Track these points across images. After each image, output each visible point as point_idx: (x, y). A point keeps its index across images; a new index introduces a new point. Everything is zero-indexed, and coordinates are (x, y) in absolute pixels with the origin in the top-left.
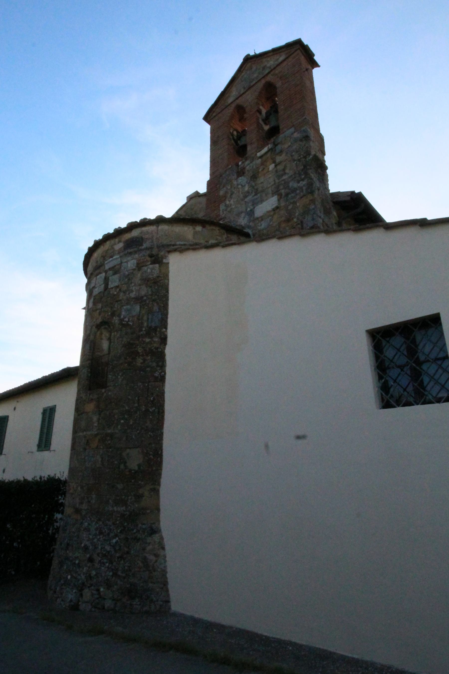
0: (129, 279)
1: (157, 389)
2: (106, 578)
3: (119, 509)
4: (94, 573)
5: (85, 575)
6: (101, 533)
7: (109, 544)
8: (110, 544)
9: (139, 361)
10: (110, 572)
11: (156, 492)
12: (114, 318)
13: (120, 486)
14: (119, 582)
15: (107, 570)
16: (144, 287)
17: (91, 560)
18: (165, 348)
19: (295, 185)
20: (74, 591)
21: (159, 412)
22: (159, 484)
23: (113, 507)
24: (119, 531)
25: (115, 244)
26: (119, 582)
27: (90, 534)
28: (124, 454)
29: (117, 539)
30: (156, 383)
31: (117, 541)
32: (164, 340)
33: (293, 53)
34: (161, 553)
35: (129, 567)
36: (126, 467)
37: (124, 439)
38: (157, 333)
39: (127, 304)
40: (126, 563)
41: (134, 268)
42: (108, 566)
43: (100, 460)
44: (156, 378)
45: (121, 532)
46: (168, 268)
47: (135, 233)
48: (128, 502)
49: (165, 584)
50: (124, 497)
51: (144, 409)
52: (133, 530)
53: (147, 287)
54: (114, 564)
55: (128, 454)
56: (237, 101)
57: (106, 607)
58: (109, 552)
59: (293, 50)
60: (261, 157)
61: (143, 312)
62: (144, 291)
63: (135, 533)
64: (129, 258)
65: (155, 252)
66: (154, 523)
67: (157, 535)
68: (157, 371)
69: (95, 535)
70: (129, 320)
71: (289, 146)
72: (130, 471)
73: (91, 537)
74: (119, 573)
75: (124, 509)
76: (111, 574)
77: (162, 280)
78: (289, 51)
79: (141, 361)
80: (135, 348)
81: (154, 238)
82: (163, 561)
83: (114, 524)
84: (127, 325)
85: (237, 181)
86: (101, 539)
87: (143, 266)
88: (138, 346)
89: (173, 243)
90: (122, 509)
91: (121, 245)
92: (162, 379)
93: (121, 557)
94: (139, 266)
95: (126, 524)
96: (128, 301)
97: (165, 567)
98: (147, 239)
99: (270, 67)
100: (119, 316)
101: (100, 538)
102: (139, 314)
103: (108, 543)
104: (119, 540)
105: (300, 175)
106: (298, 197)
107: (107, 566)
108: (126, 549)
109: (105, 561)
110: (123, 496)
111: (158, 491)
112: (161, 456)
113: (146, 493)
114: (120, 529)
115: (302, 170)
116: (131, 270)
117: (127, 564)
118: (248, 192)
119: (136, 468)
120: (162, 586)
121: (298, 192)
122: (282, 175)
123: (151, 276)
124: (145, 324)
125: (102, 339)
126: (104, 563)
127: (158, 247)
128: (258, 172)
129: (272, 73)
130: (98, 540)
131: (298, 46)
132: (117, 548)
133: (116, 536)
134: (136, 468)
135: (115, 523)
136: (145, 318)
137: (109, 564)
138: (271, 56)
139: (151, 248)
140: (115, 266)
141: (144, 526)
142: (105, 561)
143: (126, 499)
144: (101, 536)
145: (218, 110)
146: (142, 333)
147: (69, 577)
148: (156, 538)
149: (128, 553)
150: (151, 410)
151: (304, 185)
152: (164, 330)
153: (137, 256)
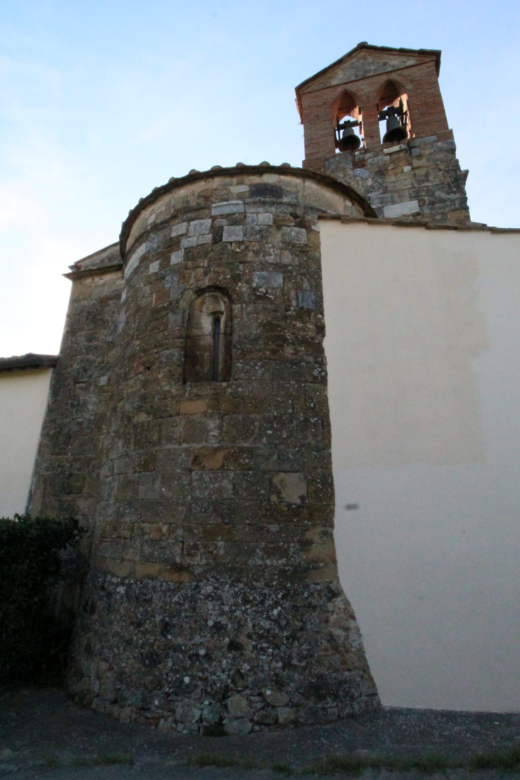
0: (262, 237)
1: (318, 393)
2: (272, 673)
3: (275, 563)
4: (246, 667)
5: (227, 673)
6: (246, 601)
7: (267, 617)
8: (269, 618)
9: (289, 351)
10: (277, 662)
11: (328, 535)
12: (240, 284)
13: (274, 528)
14: (296, 676)
15: (272, 660)
16: (287, 253)
17: (234, 646)
18: (323, 340)
19: (444, 196)
20: (207, 703)
21: (322, 423)
22: (332, 526)
23: (263, 559)
24: (280, 596)
25: (231, 185)
26: (296, 676)
27: (223, 604)
28: (275, 480)
29: (279, 608)
30: (316, 385)
31: (281, 611)
32: (321, 329)
33: (428, 62)
34: (352, 624)
35: (308, 650)
36: (281, 500)
37: (275, 457)
38: (311, 318)
39: (262, 269)
40: (302, 645)
41: (271, 223)
42: (272, 653)
43: (230, 487)
44: (315, 378)
45: (283, 597)
46: (318, 238)
47: (269, 179)
48: (290, 552)
49: (366, 669)
50: (282, 543)
51: (302, 419)
52: (303, 593)
53: (292, 255)
54: (283, 648)
55: (282, 481)
56: (345, 86)
57: (281, 720)
58: (268, 631)
59: (428, 60)
60: (390, 154)
61: (290, 285)
62: (287, 258)
63: (307, 598)
64: (261, 210)
65: (299, 212)
66: (331, 582)
67: (339, 599)
68: (315, 368)
69: (236, 604)
70: (267, 291)
71: (432, 154)
72: (289, 505)
73: (226, 608)
74: (295, 662)
75: (285, 563)
76: (280, 664)
77: (312, 251)
78: (421, 58)
79: (292, 351)
80: (281, 331)
81: (300, 194)
82: (356, 636)
83: (267, 585)
84: (264, 297)
85: (353, 171)
86: (249, 611)
87: (284, 226)
88: (285, 329)
89: (324, 209)
90: (280, 562)
91: (244, 188)
92: (324, 380)
93: (293, 637)
94: (278, 224)
95: (289, 585)
96: (264, 266)
97: (361, 644)
98: (288, 191)
99: (393, 66)
100: (249, 282)
101: (247, 609)
102: (283, 287)
103: (265, 616)
104: (283, 611)
105: (450, 187)
106: (448, 209)
107: (271, 654)
108: (299, 624)
109: (265, 645)
110: (280, 542)
111: (332, 535)
112: (331, 485)
113: (317, 538)
114: (281, 594)
115: (453, 182)
116: (265, 225)
117: (304, 647)
118: (372, 187)
119: (298, 501)
120: (361, 672)
121: (448, 203)
122: (424, 181)
123: (297, 242)
124: (294, 303)
125: (201, 311)
126: (262, 649)
127: (305, 207)
128: (387, 170)
129: (399, 72)
130: (245, 612)
131: (434, 58)
132: (283, 623)
133: (276, 604)
134: (298, 501)
135: (271, 584)
136: (293, 294)
137: (273, 649)
138: (395, 55)
139: (294, 205)
140: (234, 214)
141: (319, 587)
142: (265, 645)
143: (286, 547)
144: (248, 606)
145: (314, 86)
146: (290, 313)
147: (187, 680)
148: (338, 601)
149: (302, 629)
150: (312, 421)
151: (457, 199)
152: (320, 316)
153: (273, 209)
